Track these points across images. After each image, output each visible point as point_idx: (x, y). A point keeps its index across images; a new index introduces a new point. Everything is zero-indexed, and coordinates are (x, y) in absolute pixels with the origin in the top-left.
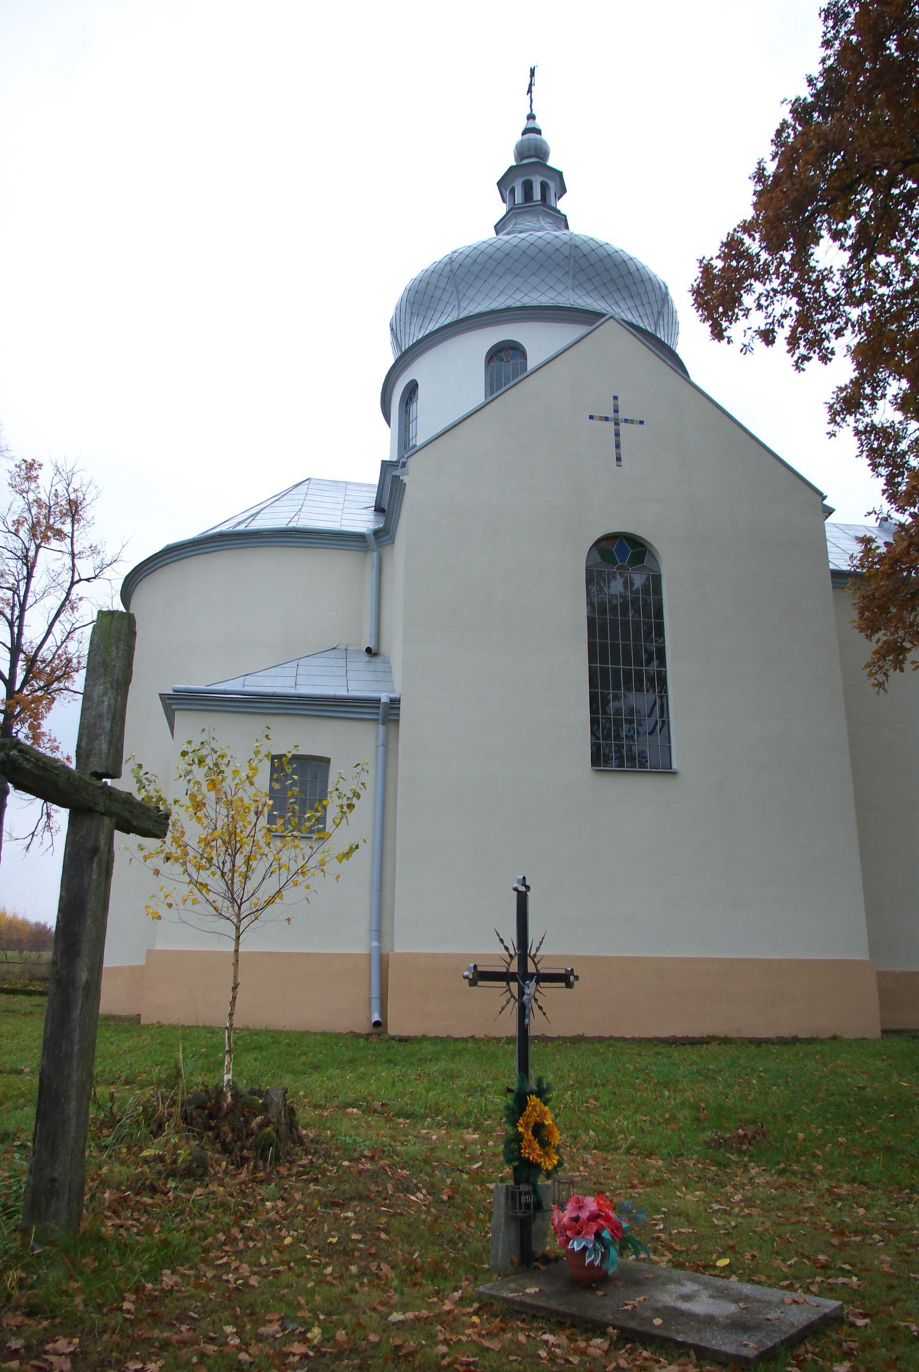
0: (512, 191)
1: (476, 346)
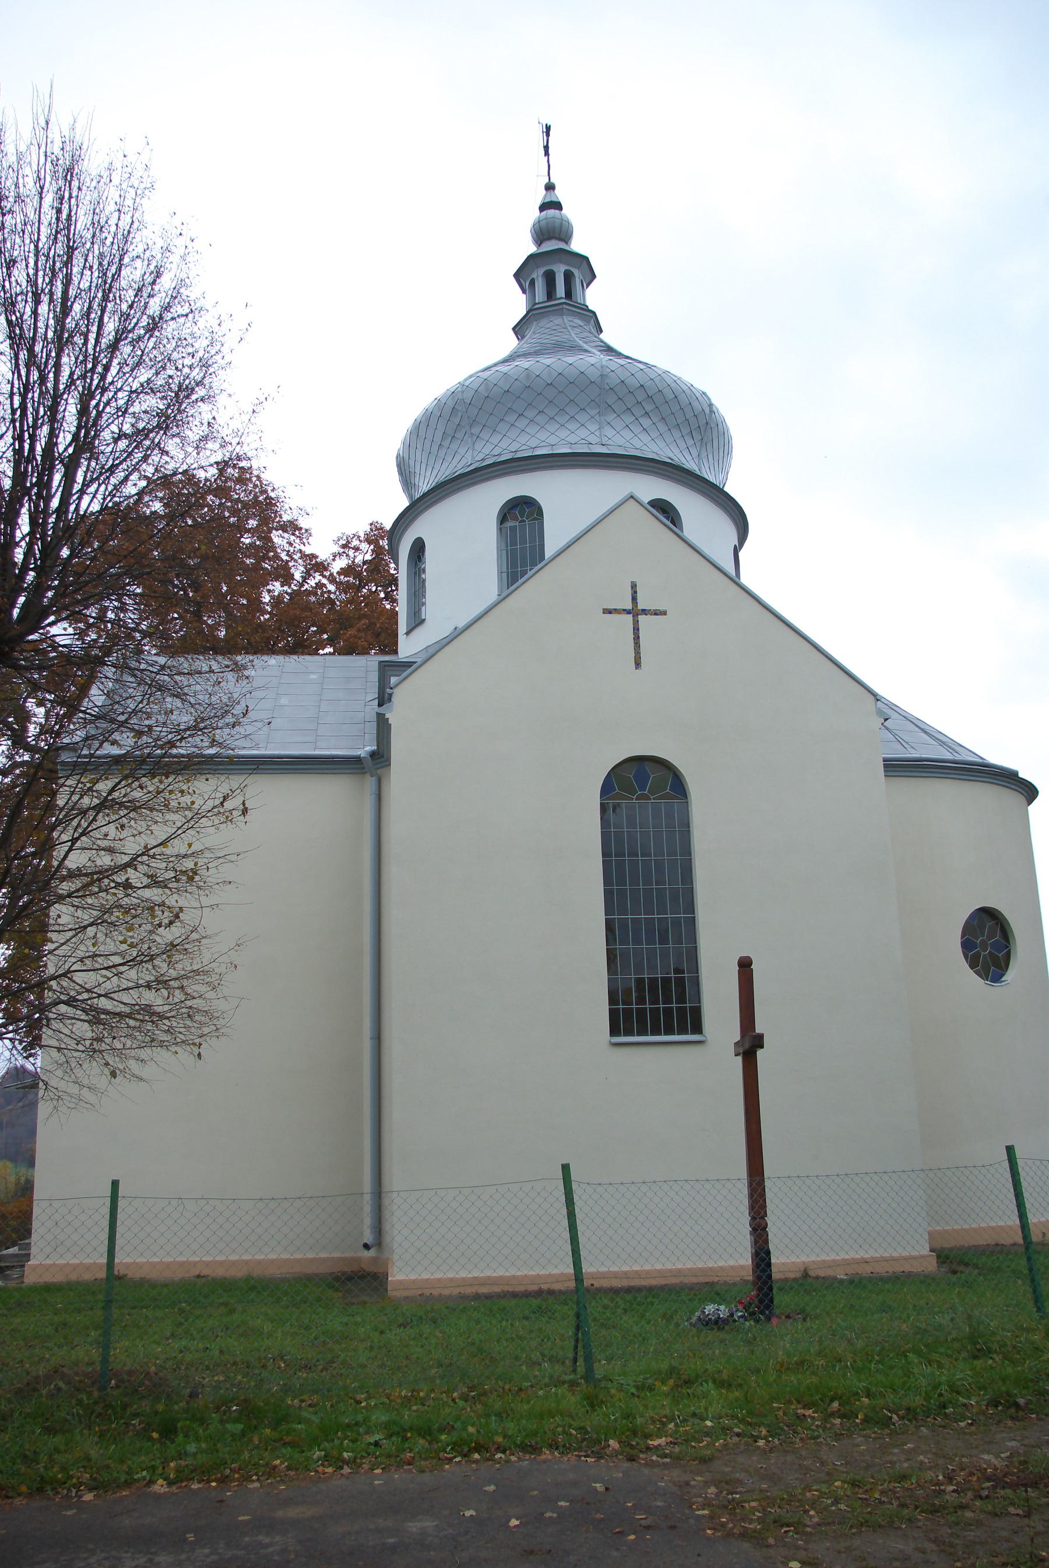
0: (532, 283)
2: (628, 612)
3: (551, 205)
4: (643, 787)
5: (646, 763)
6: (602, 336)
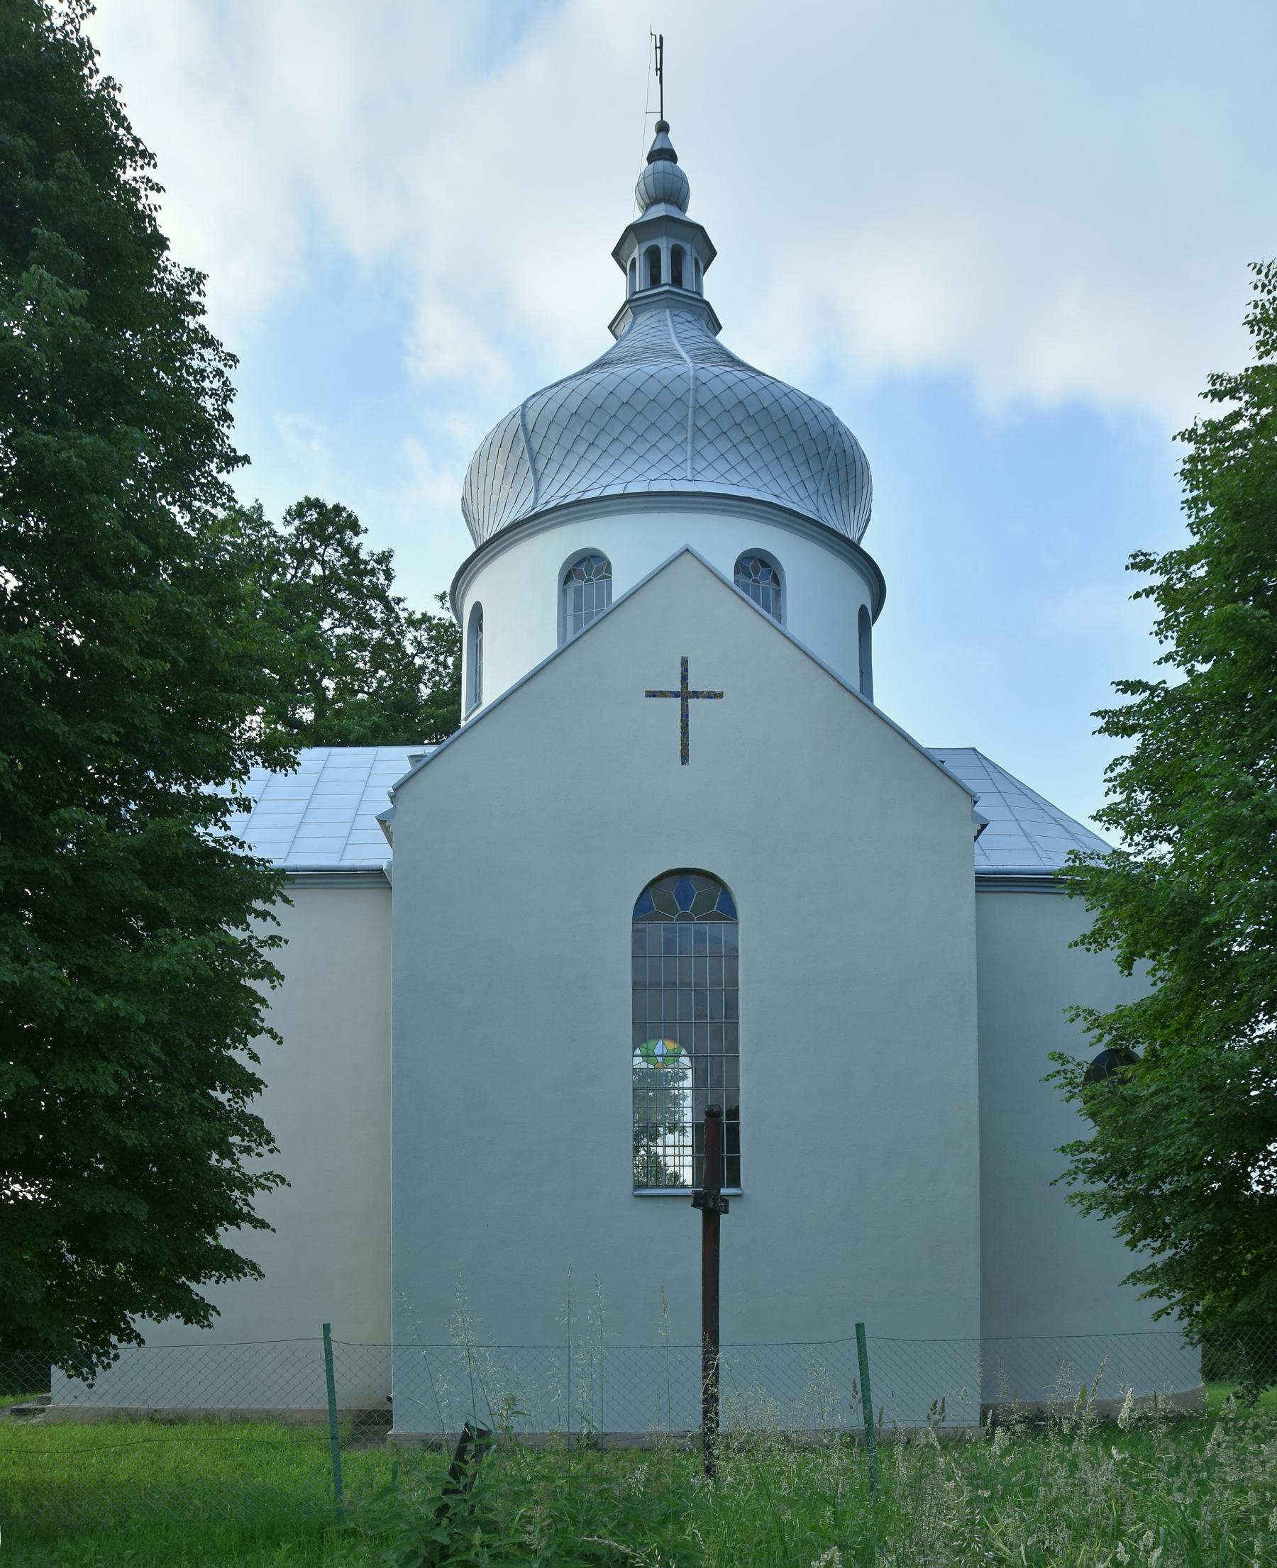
1: (549, 552)
2: (676, 695)
3: (663, 154)
4: (685, 906)
5: (691, 877)
6: (720, 338)
